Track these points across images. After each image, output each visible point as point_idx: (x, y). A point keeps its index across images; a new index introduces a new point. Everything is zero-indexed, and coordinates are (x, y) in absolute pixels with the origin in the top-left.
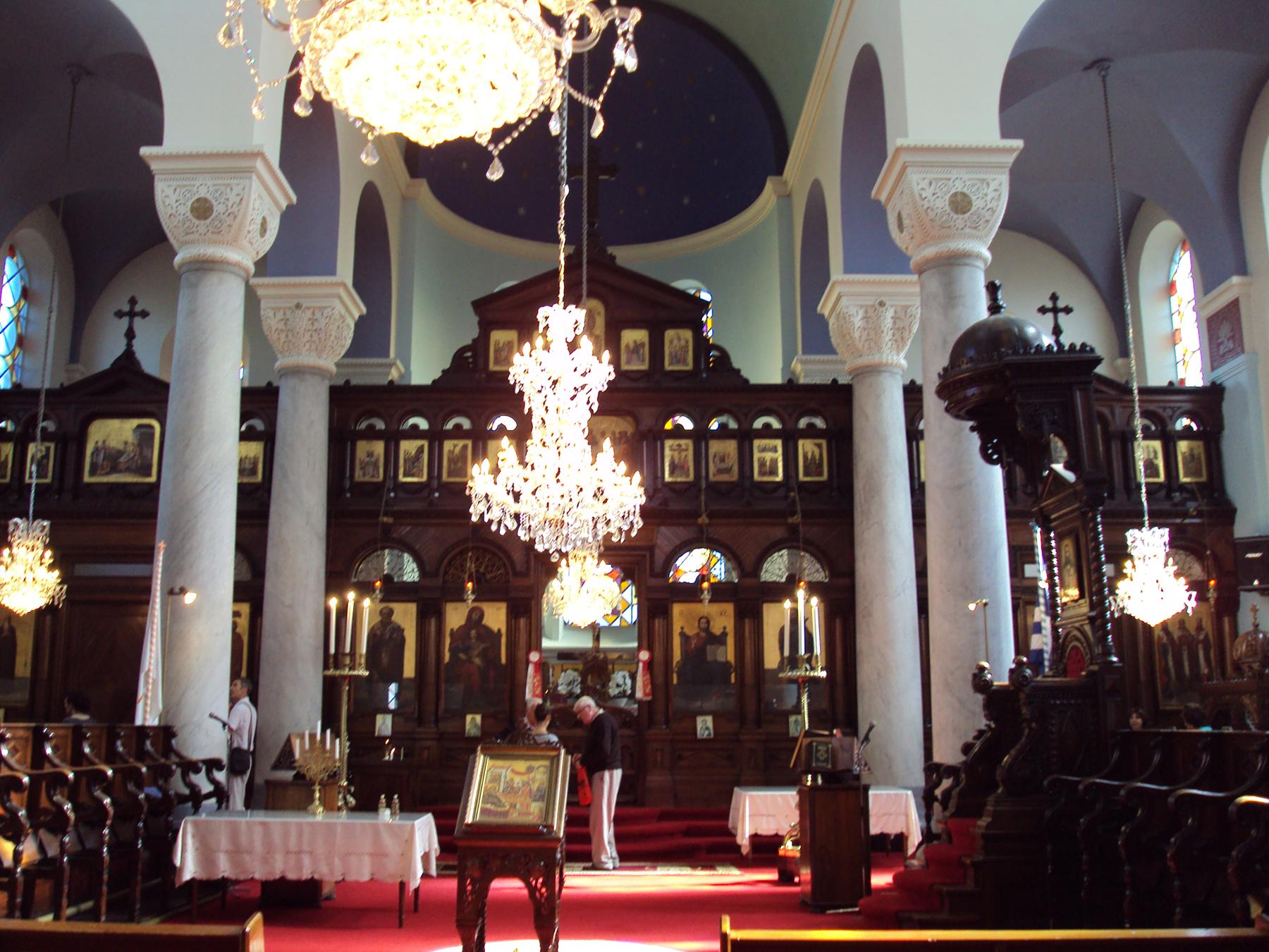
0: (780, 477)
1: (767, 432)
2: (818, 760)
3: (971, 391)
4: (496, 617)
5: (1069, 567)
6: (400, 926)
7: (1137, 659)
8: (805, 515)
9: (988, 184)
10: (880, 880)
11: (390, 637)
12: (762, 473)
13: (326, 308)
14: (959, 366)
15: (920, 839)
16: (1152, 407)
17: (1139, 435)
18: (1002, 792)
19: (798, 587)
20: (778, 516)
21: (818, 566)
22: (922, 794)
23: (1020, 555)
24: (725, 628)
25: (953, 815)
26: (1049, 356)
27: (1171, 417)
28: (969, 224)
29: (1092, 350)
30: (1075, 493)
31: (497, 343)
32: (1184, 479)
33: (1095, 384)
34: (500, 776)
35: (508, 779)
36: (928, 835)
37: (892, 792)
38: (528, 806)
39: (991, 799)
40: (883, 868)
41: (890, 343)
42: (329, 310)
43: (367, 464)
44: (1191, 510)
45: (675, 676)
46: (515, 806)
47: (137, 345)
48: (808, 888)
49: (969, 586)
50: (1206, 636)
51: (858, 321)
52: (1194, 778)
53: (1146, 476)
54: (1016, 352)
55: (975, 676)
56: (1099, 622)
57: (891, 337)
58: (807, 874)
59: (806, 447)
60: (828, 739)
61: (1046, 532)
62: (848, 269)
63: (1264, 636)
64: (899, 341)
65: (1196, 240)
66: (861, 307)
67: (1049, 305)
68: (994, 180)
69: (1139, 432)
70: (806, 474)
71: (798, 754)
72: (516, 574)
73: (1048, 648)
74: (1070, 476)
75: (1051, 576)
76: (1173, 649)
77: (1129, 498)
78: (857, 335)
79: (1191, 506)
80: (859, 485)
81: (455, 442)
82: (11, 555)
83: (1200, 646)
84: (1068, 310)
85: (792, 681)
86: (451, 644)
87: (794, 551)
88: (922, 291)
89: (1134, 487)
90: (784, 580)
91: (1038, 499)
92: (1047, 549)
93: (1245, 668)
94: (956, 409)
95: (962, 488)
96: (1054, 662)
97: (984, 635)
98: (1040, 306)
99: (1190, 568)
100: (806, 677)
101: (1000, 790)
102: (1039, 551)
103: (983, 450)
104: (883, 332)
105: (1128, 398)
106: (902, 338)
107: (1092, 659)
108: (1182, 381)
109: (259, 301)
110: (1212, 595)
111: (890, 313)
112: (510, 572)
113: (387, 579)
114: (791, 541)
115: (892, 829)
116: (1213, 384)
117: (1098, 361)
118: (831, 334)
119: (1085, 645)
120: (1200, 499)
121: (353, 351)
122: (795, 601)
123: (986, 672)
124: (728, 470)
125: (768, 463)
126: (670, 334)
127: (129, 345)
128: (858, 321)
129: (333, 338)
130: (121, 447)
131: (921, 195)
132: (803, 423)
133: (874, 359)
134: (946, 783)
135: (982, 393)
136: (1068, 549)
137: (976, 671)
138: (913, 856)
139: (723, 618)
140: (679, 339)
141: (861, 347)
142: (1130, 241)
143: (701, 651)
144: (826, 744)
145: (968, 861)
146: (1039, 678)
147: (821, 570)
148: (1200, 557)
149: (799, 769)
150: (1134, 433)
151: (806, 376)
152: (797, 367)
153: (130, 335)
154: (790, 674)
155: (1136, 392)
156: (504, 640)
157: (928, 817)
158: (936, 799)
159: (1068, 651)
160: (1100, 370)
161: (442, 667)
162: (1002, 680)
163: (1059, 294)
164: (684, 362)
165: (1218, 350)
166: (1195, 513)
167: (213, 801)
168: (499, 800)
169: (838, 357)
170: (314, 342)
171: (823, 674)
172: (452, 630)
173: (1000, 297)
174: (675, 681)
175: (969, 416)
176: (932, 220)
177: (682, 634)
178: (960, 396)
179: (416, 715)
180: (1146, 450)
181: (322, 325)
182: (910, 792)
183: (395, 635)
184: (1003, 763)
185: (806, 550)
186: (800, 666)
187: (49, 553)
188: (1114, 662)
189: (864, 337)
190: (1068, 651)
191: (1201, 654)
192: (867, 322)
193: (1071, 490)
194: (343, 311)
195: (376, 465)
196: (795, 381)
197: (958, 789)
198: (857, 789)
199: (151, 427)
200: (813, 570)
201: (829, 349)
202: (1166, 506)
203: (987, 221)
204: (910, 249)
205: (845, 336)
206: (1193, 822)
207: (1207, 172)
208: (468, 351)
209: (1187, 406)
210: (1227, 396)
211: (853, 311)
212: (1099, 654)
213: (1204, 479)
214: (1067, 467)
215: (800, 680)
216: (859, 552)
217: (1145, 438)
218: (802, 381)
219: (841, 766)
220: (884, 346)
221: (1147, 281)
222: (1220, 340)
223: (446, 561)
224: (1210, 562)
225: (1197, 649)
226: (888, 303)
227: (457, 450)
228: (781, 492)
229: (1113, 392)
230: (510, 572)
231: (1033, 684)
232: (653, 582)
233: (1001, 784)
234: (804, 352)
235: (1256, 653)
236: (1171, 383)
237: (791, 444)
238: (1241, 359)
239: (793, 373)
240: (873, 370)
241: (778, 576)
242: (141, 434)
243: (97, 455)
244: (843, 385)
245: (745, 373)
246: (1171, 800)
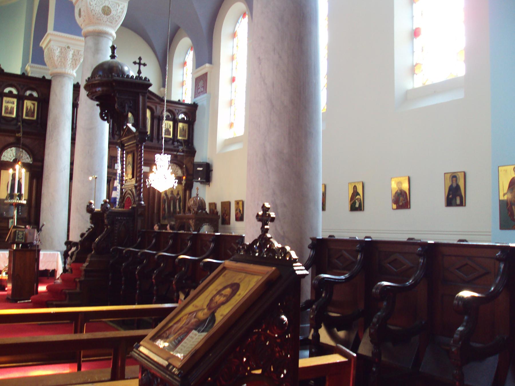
0: (14, 115)
1: (10, 94)
2: (18, 238)
3: (99, 89)
5: (129, 165)
7: (154, 204)
8: (24, 133)
9: (119, 6)
10: (42, 288)
12: (6, 113)
14: (95, 78)
15: (62, 272)
16: (171, 108)
17: (165, 118)
18: (94, 253)
19: (18, 163)
20: (12, 133)
21: (28, 156)
22: (63, 253)
23: (112, 160)
25: (73, 262)
26: (131, 80)
27: (177, 113)
28: (108, 20)
29: (149, 80)
30: (135, 136)
32: (179, 138)
33: (148, 94)
36: (65, 270)
37: (52, 252)
39: (89, 255)
40: (43, 283)
41: (70, 65)
44: (180, 150)
48: (10, 292)
49: (91, 170)
50: (180, 197)
51: (57, 53)
52: (166, 249)
53: (165, 135)
54: (118, 76)
55: (88, 206)
56: (138, 188)
57: (71, 62)
58: (10, 287)
59: (28, 104)
60: (23, 230)
61: (122, 150)
62: (56, 29)
63: (200, 198)
65: (196, 47)
66: (59, 47)
67: (138, 61)
68: (121, 4)
69: (165, 117)
70: (27, 115)
71: (9, 236)
73: (118, 197)
74: (134, 129)
75: (122, 169)
76: (168, 201)
77: (158, 142)
78: (56, 58)
79: (181, 148)
80: (50, 123)
83: (177, 201)
84: (145, 65)
85: (12, 204)
87: (18, 149)
88: (85, 45)
89: (161, 138)
90: (12, 161)
91: (120, 137)
92: (122, 158)
93: (192, 210)
94: (92, 96)
95: (92, 129)
96: (120, 202)
97: (94, 190)
98: (134, 61)
99: (177, 171)
100: (17, 203)
101: (93, 252)
102: (119, 158)
103: (101, 115)
104: (67, 59)
105: (162, 103)
106: (76, 64)
107: (134, 202)
108: (184, 101)
110: (184, 182)
114: (16, 144)
115: (51, 268)
116: (194, 103)
117: (150, 85)
118: (45, 56)
119: (132, 196)
120: (184, 146)
122: (15, 170)
123: (92, 205)
125: (9, 109)
128: (57, 53)
131: (90, 4)
132: (28, 93)
133: (62, 70)
134: (73, 249)
135: (103, 91)
136: (130, 158)
137: (88, 204)
138: (58, 279)
141: (57, 64)
142: (172, 45)
144: (23, 231)
145: (78, 280)
146: (114, 208)
147: (29, 158)
148: (181, 168)
149: (9, 242)
150: (163, 117)
151: (31, 73)
152: (28, 68)
154: (10, 201)
155: (165, 101)
157: (65, 263)
158: (68, 255)
159: (126, 198)
160: (151, 89)
162: (98, 209)
163: (142, 57)
166: (181, 151)
169: (47, 67)
171: (25, 202)
173: (115, 52)
175: (97, 99)
176: (93, 15)
178: (94, 90)
180: (167, 125)
182: (59, 253)
184: (95, 242)
185: (23, 149)
186: (14, 198)
190: (126, 198)
192: (61, 54)
193: (134, 135)
196: (26, 74)
197: (77, 252)
198: (35, 251)
200: (27, 158)
201: (43, 63)
202: (171, 147)
203: (117, 21)
204: (82, 25)
205: (51, 58)
207: (204, 24)
209: (184, 110)
210: (198, 108)
211: (55, 48)
213: (186, 138)
214: (133, 125)
215: (14, 204)
216: (47, 151)
217: (166, 120)
218: (30, 75)
219: (29, 241)
220: (67, 66)
221: (177, 60)
224: (185, 170)
225: (176, 202)
226: (71, 48)
228: (15, 122)
229: (157, 100)
231: (110, 211)
233: (93, 249)
234: (32, 62)
235: (196, 204)
236: (179, 100)
239: (26, 71)
240: (61, 75)
241: (9, 158)
246: (156, 257)
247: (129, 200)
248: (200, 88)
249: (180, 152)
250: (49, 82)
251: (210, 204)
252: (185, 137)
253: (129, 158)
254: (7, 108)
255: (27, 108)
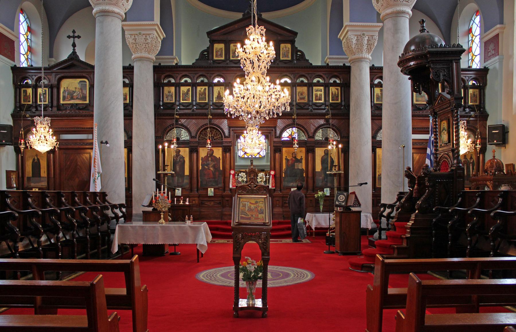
1: (318, 84)
4: (218, 153)
5: (444, 131)
6: (198, 262)
11: (180, 161)
12: (316, 100)
13: (150, 34)
14: (409, 53)
20: (321, 116)
24: (302, 157)
27: (468, 80)
29: (462, 46)
31: (216, 49)
34: (246, 205)
35: (249, 206)
38: (258, 216)
41: (366, 50)
42: (152, 35)
43: (168, 96)
45: (283, 174)
46: (253, 216)
47: (77, 49)
50: (473, 161)
57: (366, 48)
64: (369, 50)
66: (356, 35)
70: (332, 100)
72: (225, 137)
78: (353, 46)
81: (201, 87)
82: (37, 131)
83: (471, 164)
86: (201, 163)
104: (363, 45)
106: (371, 48)
109: (125, 32)
111: (366, 38)
112: (223, 136)
113: (178, 139)
116: (485, 67)
121: (161, 53)
124: (304, 98)
126: (282, 46)
127: (74, 50)
128: (354, 41)
129: (154, 46)
130: (74, 90)
139: (301, 153)
140: (286, 48)
141: (355, 51)
143: (293, 165)
153: (74, 45)
156: (221, 161)
161: (199, 171)
164: (288, 57)
165: (488, 54)
166: (474, 116)
167: (123, 219)
168: (247, 214)
170: (147, 48)
172: (202, 158)
174: (283, 176)
177: (286, 159)
179: (190, 189)
181: (150, 41)
183: (181, 160)
187: (51, 130)
188: (461, 166)
189: (357, 47)
191: (471, 167)
194: (157, 36)
195: (172, 96)
199: (85, 82)
206: (500, 221)
208: (205, 52)
209: (473, 76)
210: (489, 72)
211: (352, 37)
212: (455, 163)
222: (489, 51)
223: (199, 132)
227: (202, 90)
230: (223, 136)
232: (276, 140)
237: (327, 88)
238: (497, 57)
240: (360, 60)
242: (82, 84)
243: (65, 93)
244: (347, 66)
245: (310, 61)
247: (445, 164)
248: (490, 51)
249: (472, 118)
250: (349, 67)
251: (507, 165)
252: (477, 102)
253: (444, 124)
254: (316, 96)
255: (332, 94)
